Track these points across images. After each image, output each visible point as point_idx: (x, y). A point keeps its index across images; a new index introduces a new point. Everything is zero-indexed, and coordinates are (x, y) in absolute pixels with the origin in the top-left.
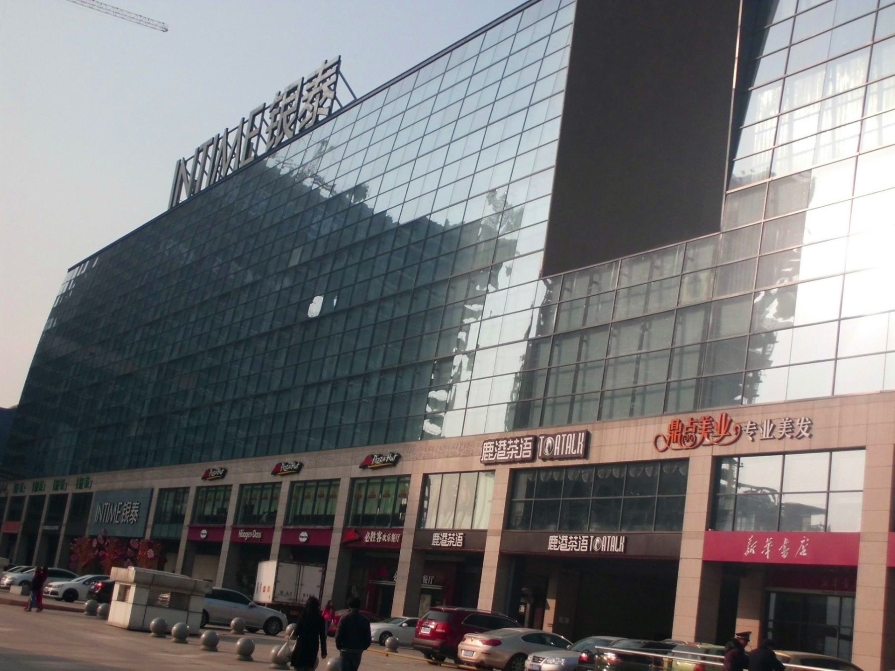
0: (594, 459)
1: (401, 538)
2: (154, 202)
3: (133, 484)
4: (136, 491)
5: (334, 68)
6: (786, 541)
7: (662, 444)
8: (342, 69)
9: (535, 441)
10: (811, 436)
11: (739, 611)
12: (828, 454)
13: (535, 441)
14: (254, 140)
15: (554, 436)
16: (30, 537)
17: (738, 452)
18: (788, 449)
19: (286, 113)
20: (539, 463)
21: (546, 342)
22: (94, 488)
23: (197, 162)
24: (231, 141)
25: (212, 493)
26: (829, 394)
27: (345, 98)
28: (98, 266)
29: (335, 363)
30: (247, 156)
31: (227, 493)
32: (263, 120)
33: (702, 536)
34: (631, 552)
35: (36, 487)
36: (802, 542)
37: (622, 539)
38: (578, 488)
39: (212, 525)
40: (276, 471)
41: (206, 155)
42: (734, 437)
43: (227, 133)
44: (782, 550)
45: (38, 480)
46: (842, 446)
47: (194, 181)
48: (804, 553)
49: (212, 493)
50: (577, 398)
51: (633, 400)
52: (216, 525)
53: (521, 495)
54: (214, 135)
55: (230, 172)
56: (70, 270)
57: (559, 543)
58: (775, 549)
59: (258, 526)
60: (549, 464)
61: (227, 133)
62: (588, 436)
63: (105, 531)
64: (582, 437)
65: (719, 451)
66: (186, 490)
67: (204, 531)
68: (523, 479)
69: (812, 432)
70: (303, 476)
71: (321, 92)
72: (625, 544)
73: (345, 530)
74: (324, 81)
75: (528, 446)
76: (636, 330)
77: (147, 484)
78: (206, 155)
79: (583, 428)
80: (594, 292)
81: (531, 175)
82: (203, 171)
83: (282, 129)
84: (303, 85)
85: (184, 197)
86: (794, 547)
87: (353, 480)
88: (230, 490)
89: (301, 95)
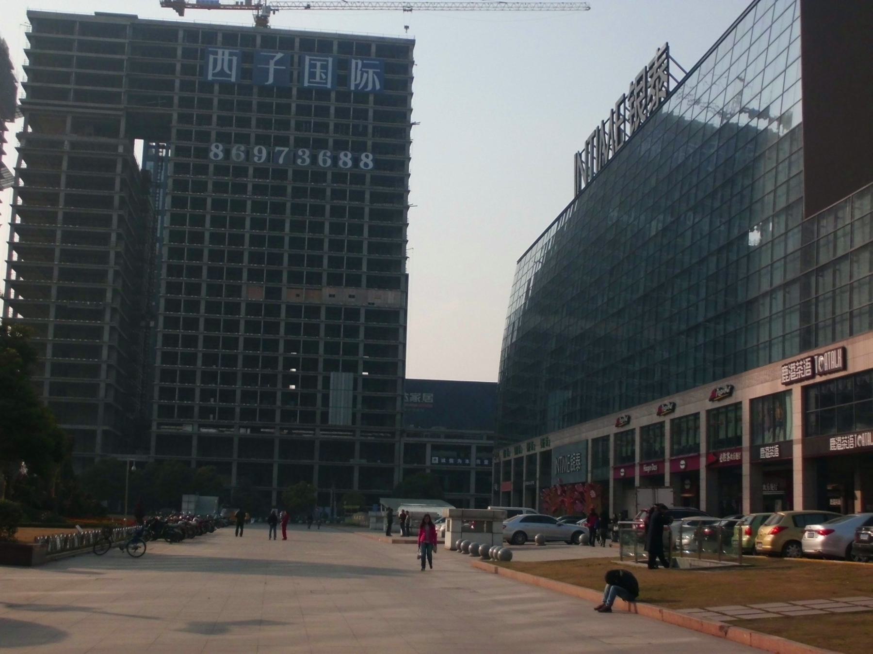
1: (741, 455)
2: (562, 193)
3: (576, 438)
4: (577, 443)
5: (664, 56)
9: (813, 362)
13: (813, 362)
14: (622, 127)
16: (518, 491)
19: (640, 99)
20: (818, 379)
22: (552, 446)
23: (587, 153)
25: (625, 438)
27: (680, 76)
28: (578, 210)
32: (625, 108)
35: (530, 447)
38: (846, 397)
39: (627, 464)
41: (593, 146)
43: (604, 124)
45: (544, 437)
47: (587, 168)
49: (725, 416)
50: (838, 319)
53: (813, 409)
54: (595, 128)
55: (627, 138)
56: (518, 262)
57: (837, 444)
60: (824, 378)
61: (604, 124)
62: (844, 351)
64: (840, 351)
67: (683, 462)
68: (813, 393)
70: (678, 414)
71: (659, 77)
75: (808, 365)
77: (584, 436)
78: (593, 146)
80: (839, 226)
82: (593, 158)
83: (638, 115)
84: (647, 73)
85: (583, 186)
87: (708, 412)
88: (741, 408)
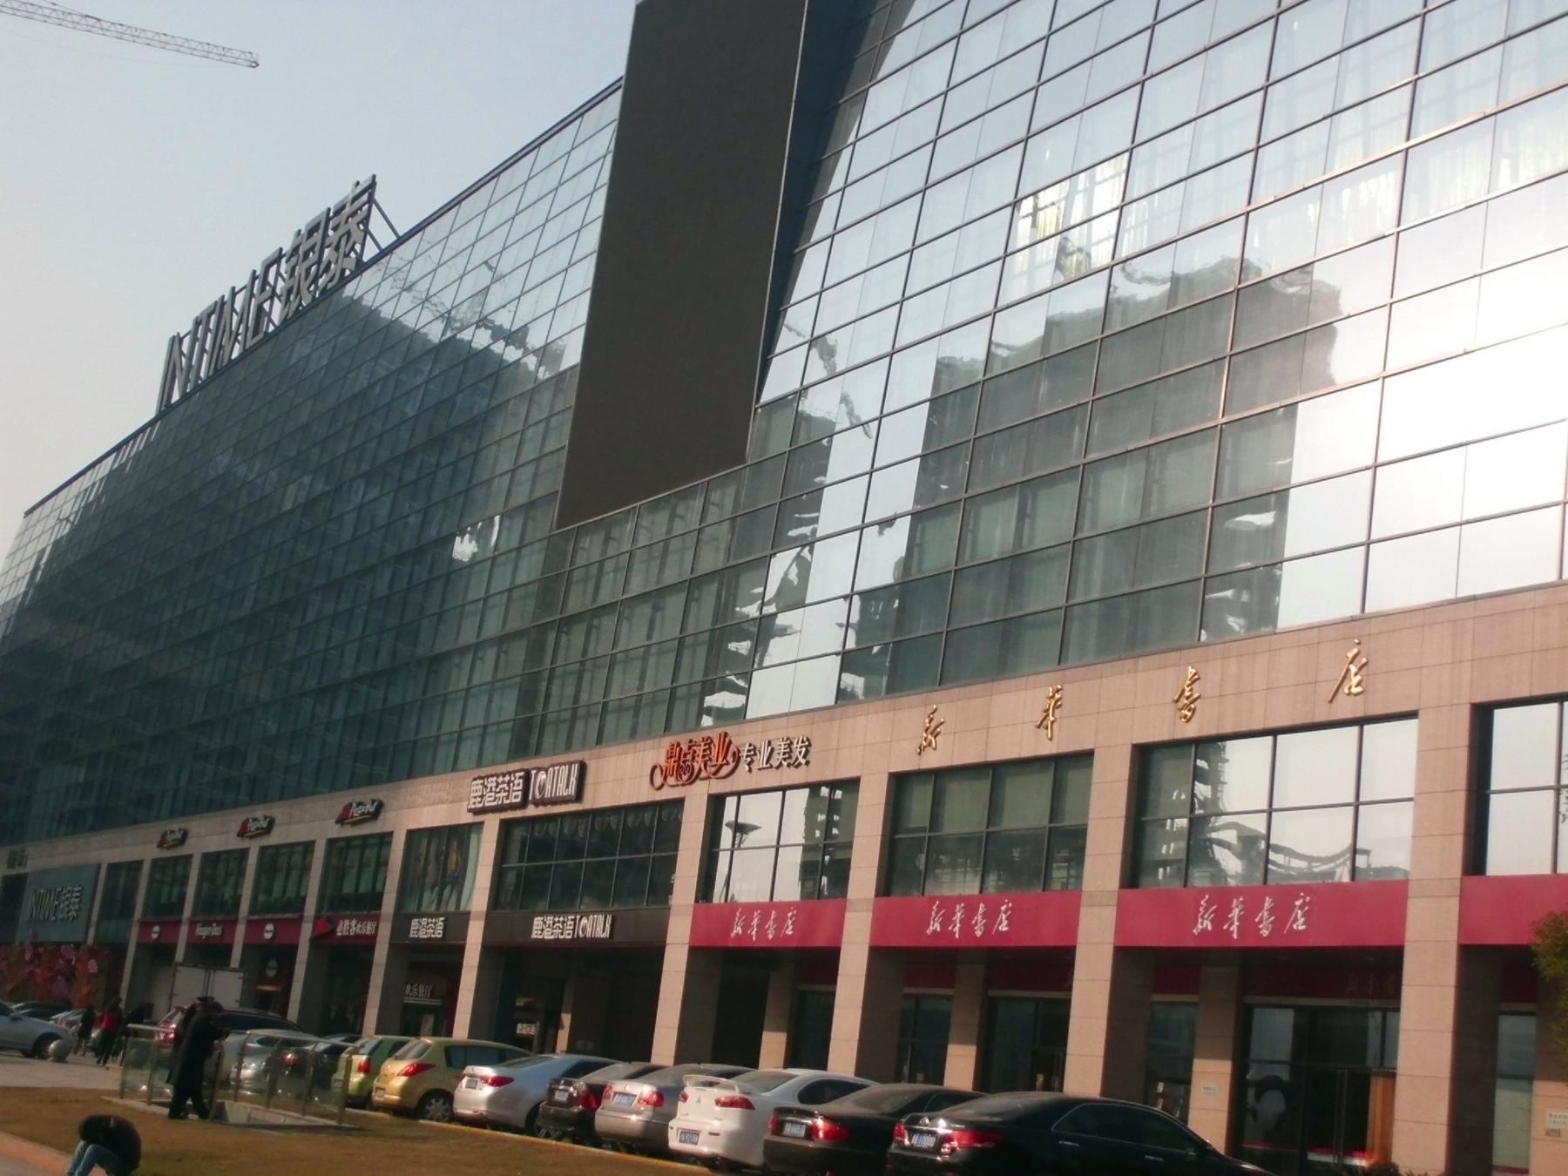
0: (589, 803)
2: (137, 404)
5: (365, 197)
6: (1268, 903)
7: (658, 780)
8: (379, 196)
9: (527, 779)
10: (807, 763)
11: (767, 1022)
12: (1269, 739)
13: (527, 779)
14: (266, 306)
15: (546, 770)
17: (735, 789)
18: (785, 783)
20: (531, 811)
21: (681, 591)
22: (30, 866)
23: (194, 340)
24: (238, 306)
25: (170, 870)
26: (1356, 611)
27: (386, 239)
28: (158, 439)
29: (592, 583)
30: (255, 333)
31: (384, 852)
32: (278, 274)
33: (690, 911)
34: (618, 938)
36: (1298, 903)
37: (609, 918)
40: (243, 833)
41: (207, 330)
42: (732, 765)
44: (1261, 921)
45: (17, 848)
46: (1244, 728)
48: (1300, 925)
49: (357, 854)
51: (636, 715)
52: (289, 915)
53: (513, 862)
54: (217, 298)
55: (271, 328)
57: (545, 928)
58: (1247, 921)
59: (219, 918)
60: (541, 811)
61: (234, 294)
62: (583, 768)
63: (35, 935)
64: (575, 768)
65: (717, 787)
66: (139, 863)
68: (518, 833)
69: (810, 757)
70: (274, 839)
71: (349, 233)
72: (612, 926)
73: (317, 917)
74: (354, 214)
76: (645, 610)
78: (207, 330)
79: (578, 756)
80: (610, 553)
81: (1206, 50)
82: (203, 350)
85: (176, 397)
86: (1282, 913)
87: (331, 842)
88: (390, 843)
89: (325, 235)
